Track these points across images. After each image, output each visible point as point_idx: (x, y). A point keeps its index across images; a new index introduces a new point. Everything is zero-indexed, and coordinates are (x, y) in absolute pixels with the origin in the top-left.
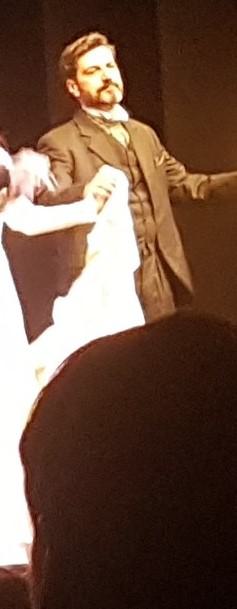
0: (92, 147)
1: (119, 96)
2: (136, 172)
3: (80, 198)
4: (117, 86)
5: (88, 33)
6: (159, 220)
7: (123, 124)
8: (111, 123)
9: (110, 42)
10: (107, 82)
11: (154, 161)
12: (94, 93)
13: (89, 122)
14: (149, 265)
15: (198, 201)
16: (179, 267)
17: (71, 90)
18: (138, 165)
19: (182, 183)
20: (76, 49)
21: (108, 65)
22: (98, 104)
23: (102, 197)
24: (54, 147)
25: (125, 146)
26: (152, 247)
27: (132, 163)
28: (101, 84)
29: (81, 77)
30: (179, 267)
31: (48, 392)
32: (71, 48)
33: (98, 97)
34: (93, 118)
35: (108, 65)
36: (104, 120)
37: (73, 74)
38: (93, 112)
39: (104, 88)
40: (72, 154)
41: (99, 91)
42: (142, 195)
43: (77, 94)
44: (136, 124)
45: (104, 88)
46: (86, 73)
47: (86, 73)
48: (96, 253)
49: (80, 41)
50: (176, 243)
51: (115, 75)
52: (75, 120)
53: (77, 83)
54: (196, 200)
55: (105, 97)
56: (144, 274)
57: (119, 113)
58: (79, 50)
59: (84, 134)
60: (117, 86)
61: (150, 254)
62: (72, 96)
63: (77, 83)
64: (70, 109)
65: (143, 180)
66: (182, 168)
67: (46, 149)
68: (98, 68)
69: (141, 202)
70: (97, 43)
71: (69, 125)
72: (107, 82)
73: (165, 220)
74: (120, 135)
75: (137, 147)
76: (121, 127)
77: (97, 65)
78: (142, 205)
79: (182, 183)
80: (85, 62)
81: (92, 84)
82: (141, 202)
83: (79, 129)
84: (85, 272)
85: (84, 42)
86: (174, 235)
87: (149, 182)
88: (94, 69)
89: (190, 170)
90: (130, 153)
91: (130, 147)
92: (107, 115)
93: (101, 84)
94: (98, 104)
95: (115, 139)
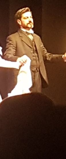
0: (23, 40)
1: (33, 27)
2: (34, 48)
3: (15, 61)
4: (32, 23)
6: (40, 62)
7: (32, 34)
9: (31, 11)
10: (30, 22)
11: (40, 46)
12: (26, 24)
13: (22, 32)
14: (37, 75)
15: (48, 61)
16: (45, 77)
17: (19, 23)
18: (35, 46)
19: (45, 55)
20: (22, 11)
22: (26, 27)
23: (22, 63)
24: (11, 40)
25: (32, 40)
26: (38, 70)
27: (34, 45)
28: (28, 22)
29: (22, 19)
30: (45, 77)
32: (20, 11)
33: (27, 26)
34: (24, 32)
36: (27, 33)
37: (20, 18)
39: (29, 23)
40: (16, 42)
41: (28, 24)
42: (36, 54)
43: (20, 24)
44: (35, 35)
45: (29, 23)
46: (24, 18)
47: (24, 18)
49: (23, 9)
50: (43, 66)
51: (32, 20)
52: (19, 32)
53: (21, 21)
54: (48, 60)
55: (29, 26)
56: (35, 76)
57: (31, 31)
58: (23, 11)
60: (32, 23)
62: (19, 24)
63: (21, 21)
64: (17, 28)
65: (36, 50)
66: (46, 50)
67: (9, 40)
68: (28, 18)
69: (35, 56)
70: (27, 11)
71: (17, 33)
72: (30, 22)
73: (42, 62)
74: (31, 37)
75: (35, 41)
76: (31, 35)
77: (27, 17)
78: (36, 62)
79: (45, 55)
80: (25, 15)
81: (26, 22)
83: (19, 34)
84: (17, 84)
85: (25, 9)
86: (44, 70)
88: (27, 18)
89: (48, 52)
90: (33, 42)
91: (33, 40)
92: (28, 31)
93: (28, 22)
94: (26, 27)
95: (29, 38)
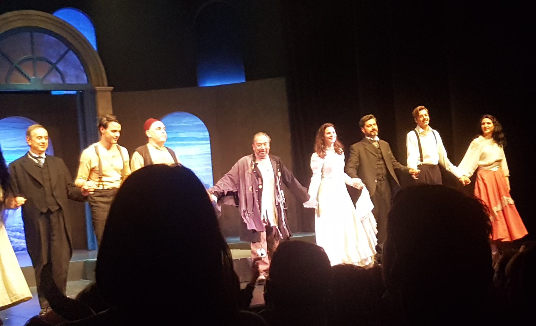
1: (377, 134)
5: (369, 114)
8: (374, 141)
10: (374, 130)
12: (369, 132)
21: (374, 124)
29: (366, 127)
31: (360, 195)
35: (374, 124)
37: (363, 126)
38: (368, 138)
48: (348, 256)
51: (376, 127)
55: (373, 134)
57: (377, 138)
59: (364, 222)
61: (244, 211)
68: (160, 128)
70: (371, 118)
71: (360, 142)
74: (376, 145)
82: (381, 168)
87: (385, 158)
91: (379, 148)
94: (370, 136)
